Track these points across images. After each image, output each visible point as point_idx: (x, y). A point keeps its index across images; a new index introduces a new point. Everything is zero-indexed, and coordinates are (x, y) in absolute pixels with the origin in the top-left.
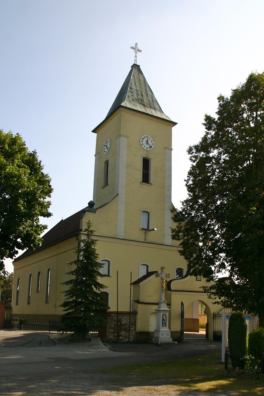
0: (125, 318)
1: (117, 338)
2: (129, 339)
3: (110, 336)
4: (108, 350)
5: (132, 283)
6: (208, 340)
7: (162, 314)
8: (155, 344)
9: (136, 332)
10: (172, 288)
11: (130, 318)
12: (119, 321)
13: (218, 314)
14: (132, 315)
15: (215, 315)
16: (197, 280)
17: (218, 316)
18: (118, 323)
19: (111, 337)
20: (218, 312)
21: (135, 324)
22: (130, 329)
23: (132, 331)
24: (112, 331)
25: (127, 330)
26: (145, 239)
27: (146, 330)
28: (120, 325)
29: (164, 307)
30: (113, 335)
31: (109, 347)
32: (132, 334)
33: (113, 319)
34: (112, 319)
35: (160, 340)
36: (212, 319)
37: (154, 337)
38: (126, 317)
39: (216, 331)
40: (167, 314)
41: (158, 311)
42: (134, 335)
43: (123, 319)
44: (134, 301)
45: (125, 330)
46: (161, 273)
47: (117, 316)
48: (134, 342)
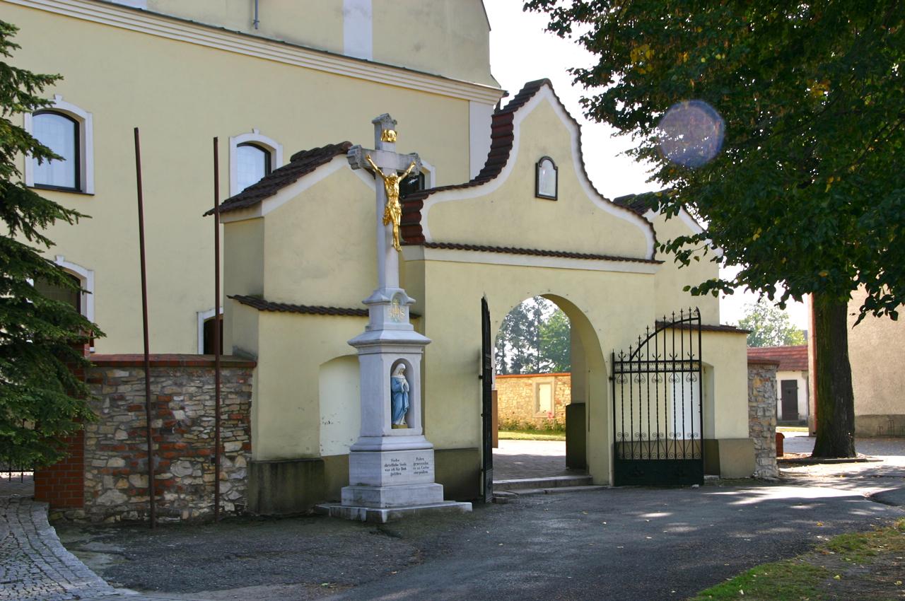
0: (192, 390)
1: (148, 498)
2: (217, 500)
3: (105, 490)
4: (100, 580)
5: (221, 201)
6: (589, 481)
7: (388, 360)
8: (358, 521)
9: (251, 464)
10: (428, 233)
11: (217, 390)
12: (157, 406)
13: (635, 359)
14: (225, 373)
15: (622, 362)
16: (537, 195)
17: (635, 367)
18: (149, 420)
19: (113, 496)
20: (635, 347)
21: (243, 420)
22: (219, 450)
23: (232, 459)
24: (119, 463)
25: (205, 456)
26: (255, 23)
27: (303, 448)
28: (167, 429)
29: (395, 325)
30: (123, 484)
31: (104, 559)
32: (230, 472)
33: (122, 398)
34: (116, 399)
35: (384, 499)
36: (609, 385)
37: (347, 484)
38: (197, 383)
39: (628, 439)
40: (415, 361)
41: (369, 346)
42: (239, 480)
43: (179, 394)
44: (237, 298)
45: (192, 453)
46: (378, 148)
47: (147, 378)
48: (244, 517)
